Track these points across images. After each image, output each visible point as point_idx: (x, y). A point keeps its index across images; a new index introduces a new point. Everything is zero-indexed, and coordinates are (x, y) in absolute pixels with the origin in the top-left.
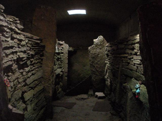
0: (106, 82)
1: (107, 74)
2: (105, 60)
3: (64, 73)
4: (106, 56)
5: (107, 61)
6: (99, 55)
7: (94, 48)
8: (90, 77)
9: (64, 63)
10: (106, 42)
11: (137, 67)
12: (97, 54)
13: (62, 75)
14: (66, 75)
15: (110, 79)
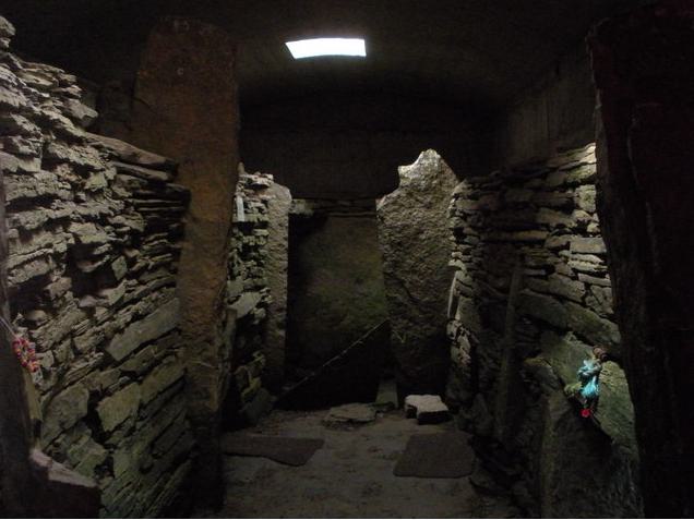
0: (455, 351)
1: (458, 317)
2: (449, 254)
3: (272, 309)
4: (453, 238)
5: (456, 258)
6: (422, 232)
7: (403, 205)
8: (386, 329)
9: (271, 267)
10: (454, 176)
11: (588, 285)
12: (412, 231)
13: (264, 321)
14: (280, 319)
15: (469, 337)
